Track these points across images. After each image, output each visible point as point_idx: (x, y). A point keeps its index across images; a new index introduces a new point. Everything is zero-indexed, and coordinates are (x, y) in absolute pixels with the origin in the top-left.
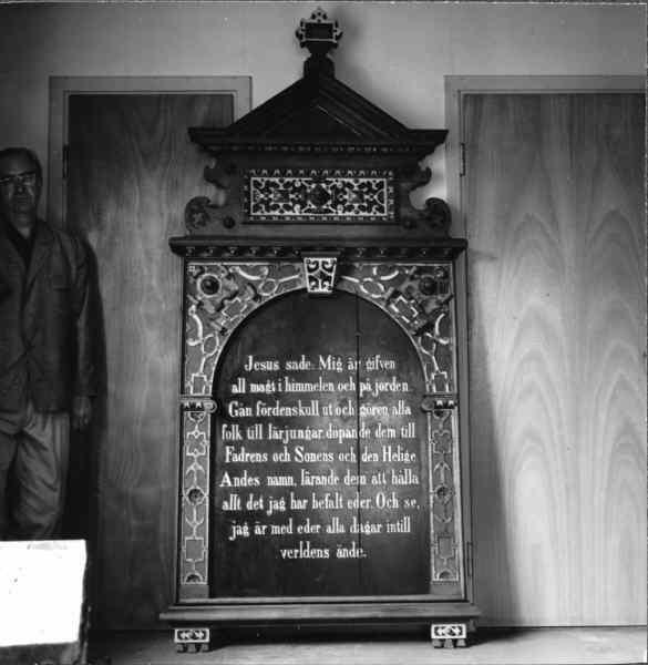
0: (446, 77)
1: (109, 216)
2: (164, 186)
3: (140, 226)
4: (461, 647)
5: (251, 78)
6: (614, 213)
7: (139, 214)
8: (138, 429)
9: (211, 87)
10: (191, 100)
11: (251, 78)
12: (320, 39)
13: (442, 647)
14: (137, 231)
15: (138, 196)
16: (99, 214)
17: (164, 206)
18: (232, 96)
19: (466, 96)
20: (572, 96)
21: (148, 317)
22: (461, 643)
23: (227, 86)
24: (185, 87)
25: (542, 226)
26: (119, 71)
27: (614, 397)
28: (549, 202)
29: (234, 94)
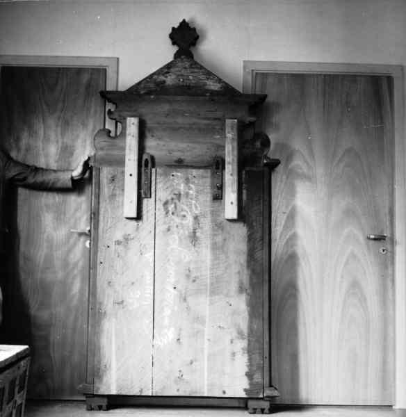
0: (244, 61)
1: (24, 142)
2: (60, 124)
3: (43, 149)
4: (266, 413)
5: (118, 59)
6: (349, 151)
7: (43, 142)
8: (39, 275)
9: (96, 64)
10: (79, 71)
11: (118, 59)
12: (185, 37)
13: (254, 413)
14: (41, 152)
15: (42, 129)
16: (18, 140)
17: (59, 136)
18: (105, 70)
19: (257, 73)
20: (325, 75)
21: (47, 206)
22: (266, 411)
23: (104, 63)
24: (79, 64)
25: (304, 157)
26: (32, 53)
27: (347, 263)
28: (309, 144)
29: (255, 72)
